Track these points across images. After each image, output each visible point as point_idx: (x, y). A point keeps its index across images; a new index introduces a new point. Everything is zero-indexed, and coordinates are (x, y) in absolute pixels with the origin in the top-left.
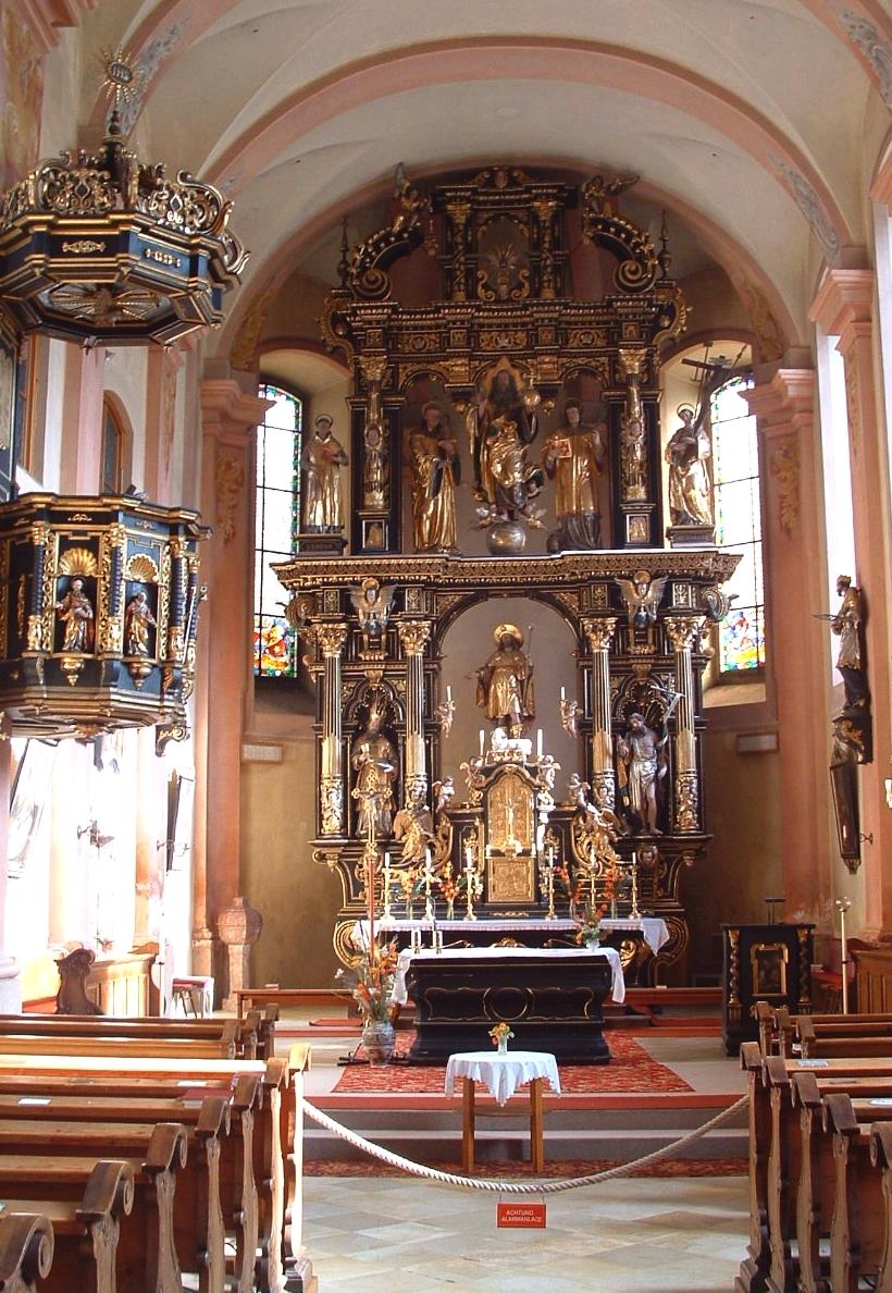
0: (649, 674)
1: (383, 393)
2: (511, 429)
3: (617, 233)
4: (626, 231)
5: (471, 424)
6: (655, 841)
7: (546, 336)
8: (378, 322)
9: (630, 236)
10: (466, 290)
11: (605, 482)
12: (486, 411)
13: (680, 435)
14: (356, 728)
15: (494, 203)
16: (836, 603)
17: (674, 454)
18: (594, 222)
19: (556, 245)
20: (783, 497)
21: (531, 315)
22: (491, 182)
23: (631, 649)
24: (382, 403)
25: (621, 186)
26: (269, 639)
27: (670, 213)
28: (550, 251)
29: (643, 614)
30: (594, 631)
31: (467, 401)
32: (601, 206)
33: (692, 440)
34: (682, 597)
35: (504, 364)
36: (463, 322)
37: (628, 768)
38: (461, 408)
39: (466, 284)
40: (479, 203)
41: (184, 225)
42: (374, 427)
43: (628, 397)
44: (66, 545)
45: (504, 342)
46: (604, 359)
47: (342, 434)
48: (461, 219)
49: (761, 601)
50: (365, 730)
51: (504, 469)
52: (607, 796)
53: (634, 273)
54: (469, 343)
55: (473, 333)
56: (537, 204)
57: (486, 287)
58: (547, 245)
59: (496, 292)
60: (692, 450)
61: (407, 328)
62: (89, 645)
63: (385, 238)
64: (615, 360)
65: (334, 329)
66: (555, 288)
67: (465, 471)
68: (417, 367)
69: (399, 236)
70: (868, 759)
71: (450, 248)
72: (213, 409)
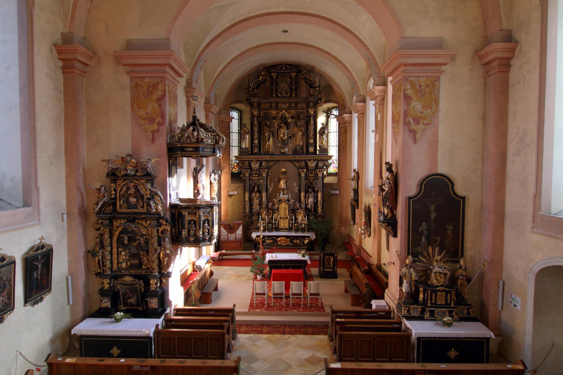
0: (313, 180)
1: (257, 117)
2: (285, 127)
3: (309, 81)
4: (312, 81)
5: (276, 125)
6: (313, 215)
7: (293, 105)
8: (256, 102)
9: (312, 82)
10: (276, 94)
11: (305, 137)
12: (280, 122)
13: (321, 129)
14: (252, 190)
15: (282, 73)
16: (353, 174)
17: (320, 134)
18: (304, 78)
19: (296, 83)
20: (343, 140)
21: (290, 100)
22: (281, 68)
23: (309, 175)
24: (257, 120)
25: (311, 70)
26: (234, 165)
27: (322, 76)
28: (294, 85)
29: (312, 168)
30: (302, 172)
31: (275, 119)
32: (306, 75)
33: (324, 130)
34: (320, 164)
35: (284, 111)
36: (275, 102)
37: (308, 200)
38: (274, 121)
39: (276, 93)
40: (279, 73)
41: (212, 142)
42: (255, 126)
43: (310, 119)
44: (189, 214)
45: (284, 106)
46: (305, 110)
47: (249, 126)
48: (275, 77)
49: (337, 145)
50: (254, 191)
51: (283, 135)
52: (303, 206)
53: (312, 91)
54: (276, 107)
55: (277, 104)
56: (292, 74)
57: (280, 94)
58: (293, 84)
59: (282, 95)
60: (324, 132)
61: (263, 102)
62: (195, 235)
63: (258, 81)
64: (308, 111)
65: (247, 102)
66: (295, 94)
67: (275, 134)
68: (265, 111)
69: (261, 81)
70: (358, 208)
71: (272, 84)
72: (220, 121)
